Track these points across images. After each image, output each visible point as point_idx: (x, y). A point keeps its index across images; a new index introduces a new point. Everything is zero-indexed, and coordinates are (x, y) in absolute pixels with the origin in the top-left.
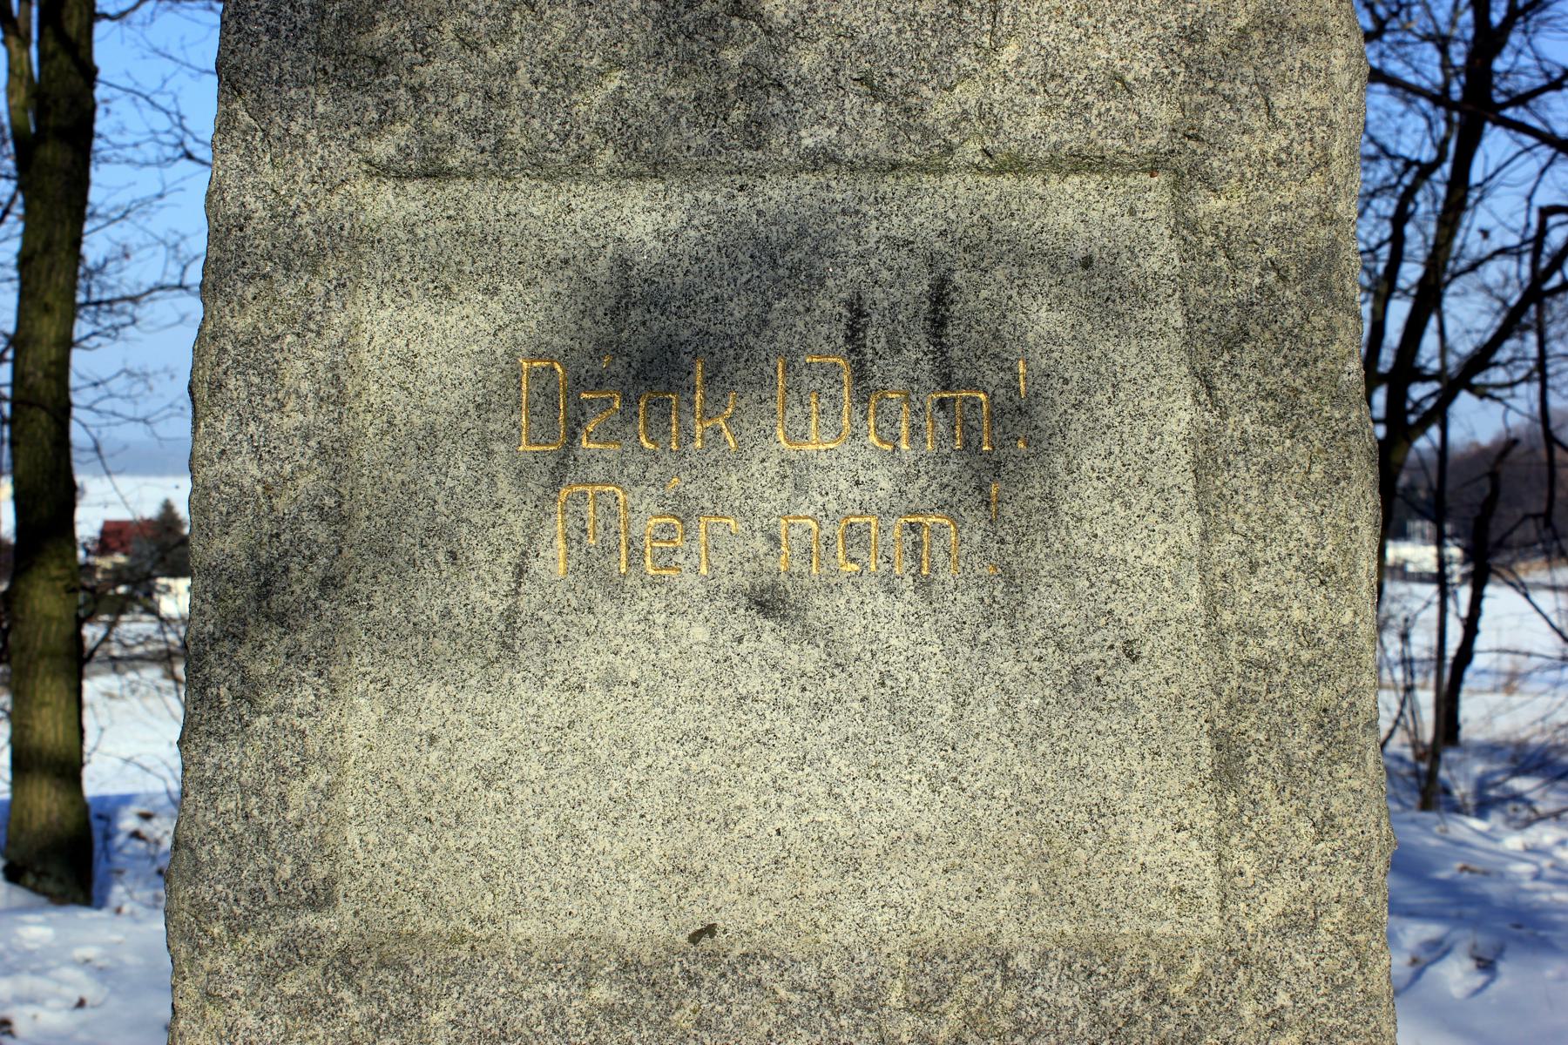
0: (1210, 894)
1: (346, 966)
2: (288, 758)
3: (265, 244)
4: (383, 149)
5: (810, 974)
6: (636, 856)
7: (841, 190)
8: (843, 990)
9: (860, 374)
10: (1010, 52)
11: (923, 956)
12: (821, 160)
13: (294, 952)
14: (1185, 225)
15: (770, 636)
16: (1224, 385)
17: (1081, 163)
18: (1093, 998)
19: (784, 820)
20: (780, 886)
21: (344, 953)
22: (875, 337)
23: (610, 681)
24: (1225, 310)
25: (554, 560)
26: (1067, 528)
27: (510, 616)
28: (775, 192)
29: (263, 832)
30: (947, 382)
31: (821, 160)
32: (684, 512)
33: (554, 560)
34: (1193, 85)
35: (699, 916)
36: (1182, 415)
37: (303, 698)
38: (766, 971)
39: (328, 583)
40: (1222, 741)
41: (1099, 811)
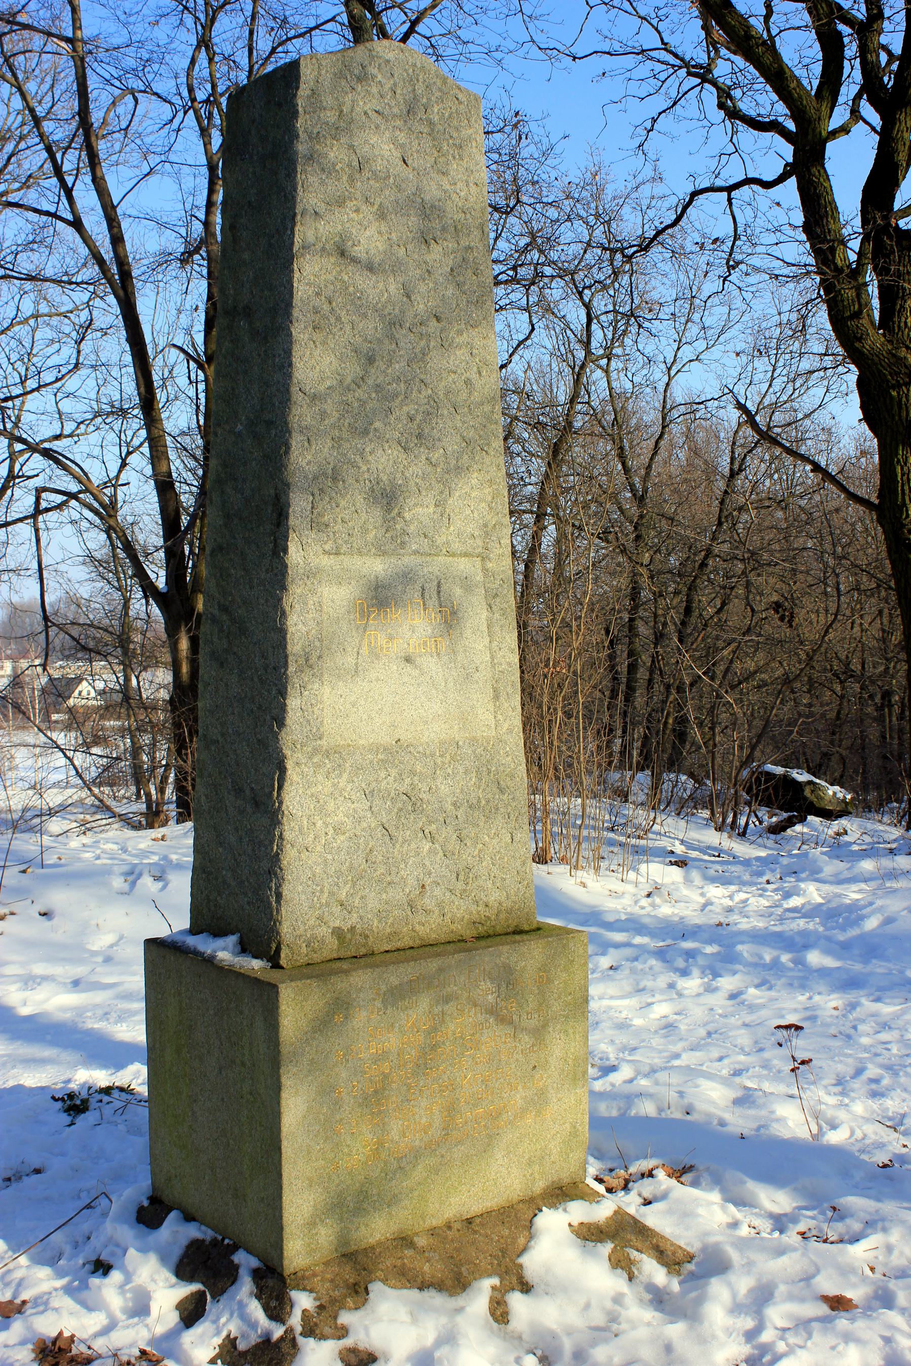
0: (493, 726)
1: (327, 754)
2: (313, 702)
3: (302, 571)
4: (327, 547)
5: (421, 749)
6: (384, 722)
7: (419, 559)
8: (428, 752)
9: (424, 605)
10: (452, 528)
11: (442, 743)
12: (416, 552)
13: (316, 751)
14: (485, 570)
15: (409, 668)
16: (494, 608)
17: (466, 555)
18: (474, 752)
19: (413, 712)
20: (412, 728)
21: (327, 751)
22: (427, 596)
23: (378, 680)
24: (853, 525)
25: (365, 650)
26: (853, 623)
27: (356, 664)
28: (406, 560)
29: (308, 721)
30: (441, 606)
31: (416, 552)
32: (391, 638)
33: (365, 650)
34: (485, 538)
35: (397, 737)
36: (484, 614)
37: (316, 686)
38: (411, 749)
39: (320, 657)
40: (495, 690)
41: (472, 707)
